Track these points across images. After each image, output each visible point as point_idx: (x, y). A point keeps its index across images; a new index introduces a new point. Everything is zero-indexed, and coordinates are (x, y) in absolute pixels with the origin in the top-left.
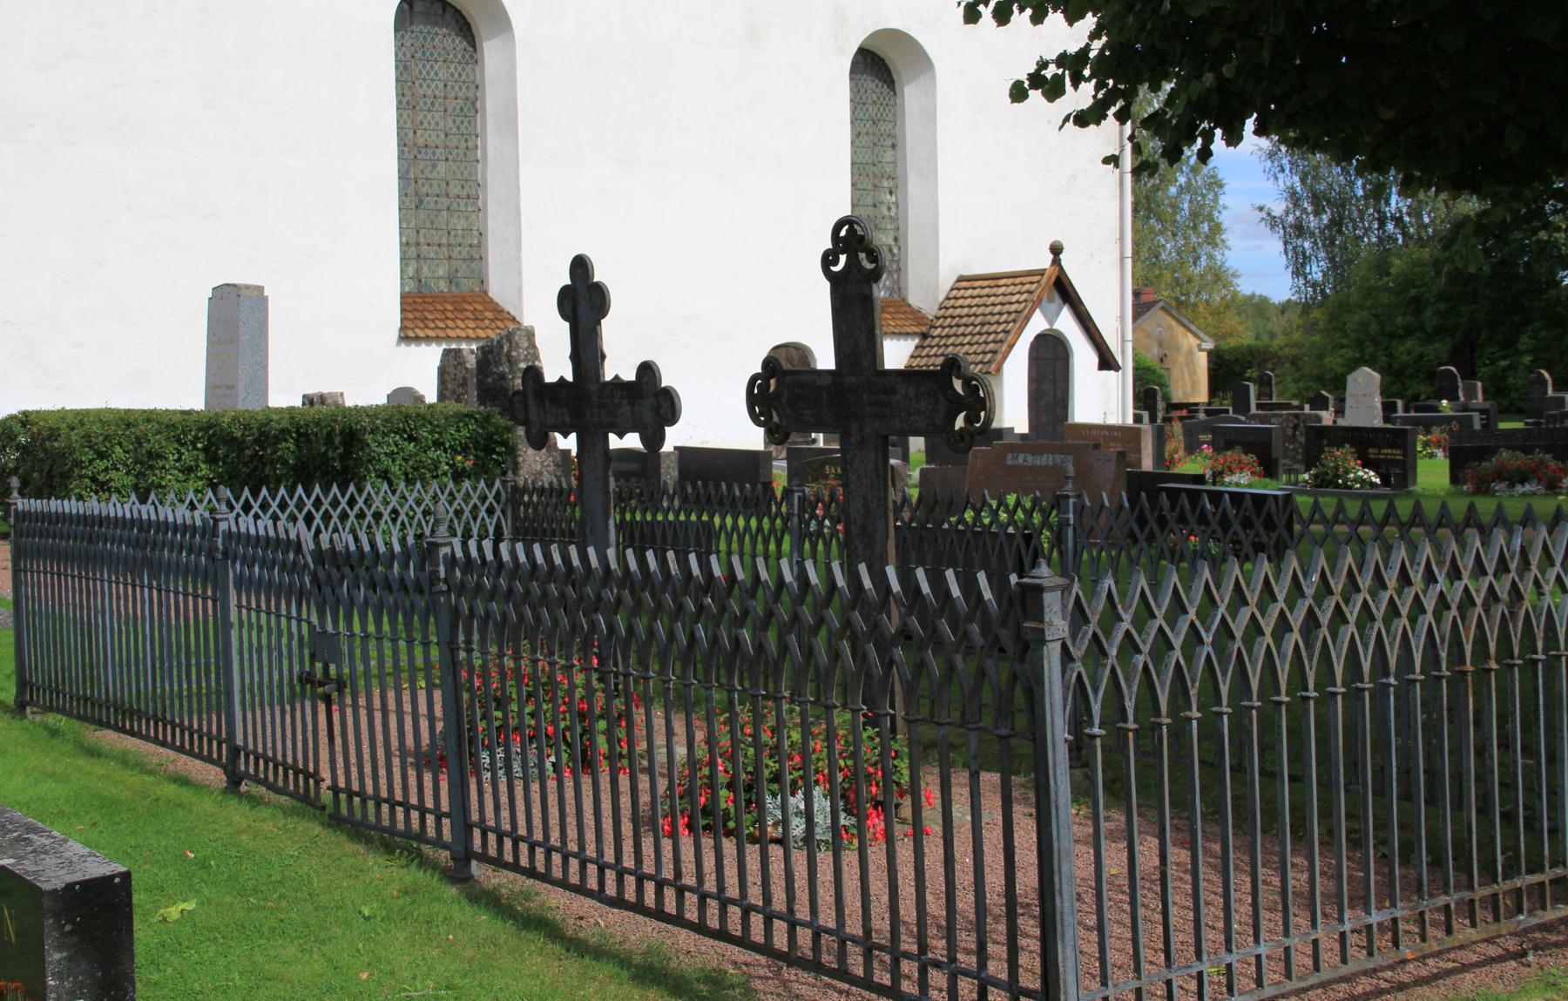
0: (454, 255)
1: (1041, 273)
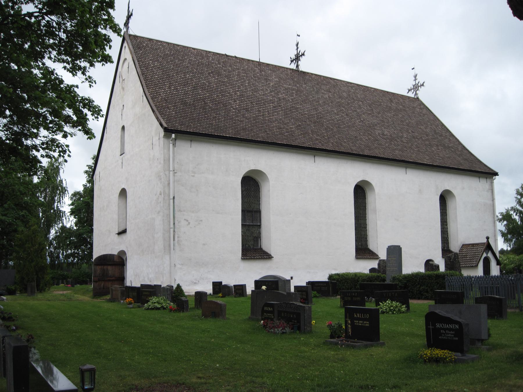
0: (362, 240)
1: (484, 243)
